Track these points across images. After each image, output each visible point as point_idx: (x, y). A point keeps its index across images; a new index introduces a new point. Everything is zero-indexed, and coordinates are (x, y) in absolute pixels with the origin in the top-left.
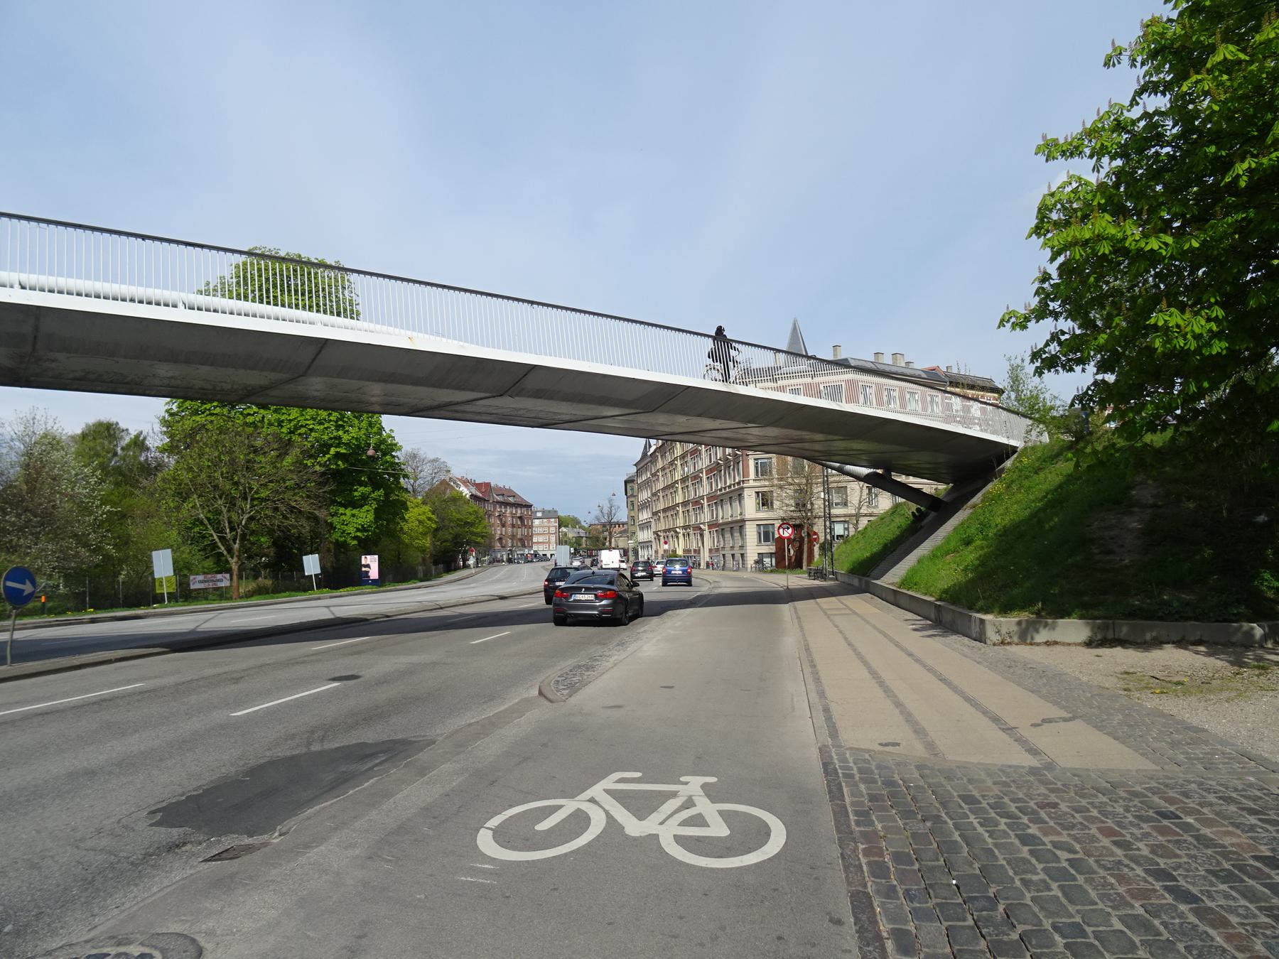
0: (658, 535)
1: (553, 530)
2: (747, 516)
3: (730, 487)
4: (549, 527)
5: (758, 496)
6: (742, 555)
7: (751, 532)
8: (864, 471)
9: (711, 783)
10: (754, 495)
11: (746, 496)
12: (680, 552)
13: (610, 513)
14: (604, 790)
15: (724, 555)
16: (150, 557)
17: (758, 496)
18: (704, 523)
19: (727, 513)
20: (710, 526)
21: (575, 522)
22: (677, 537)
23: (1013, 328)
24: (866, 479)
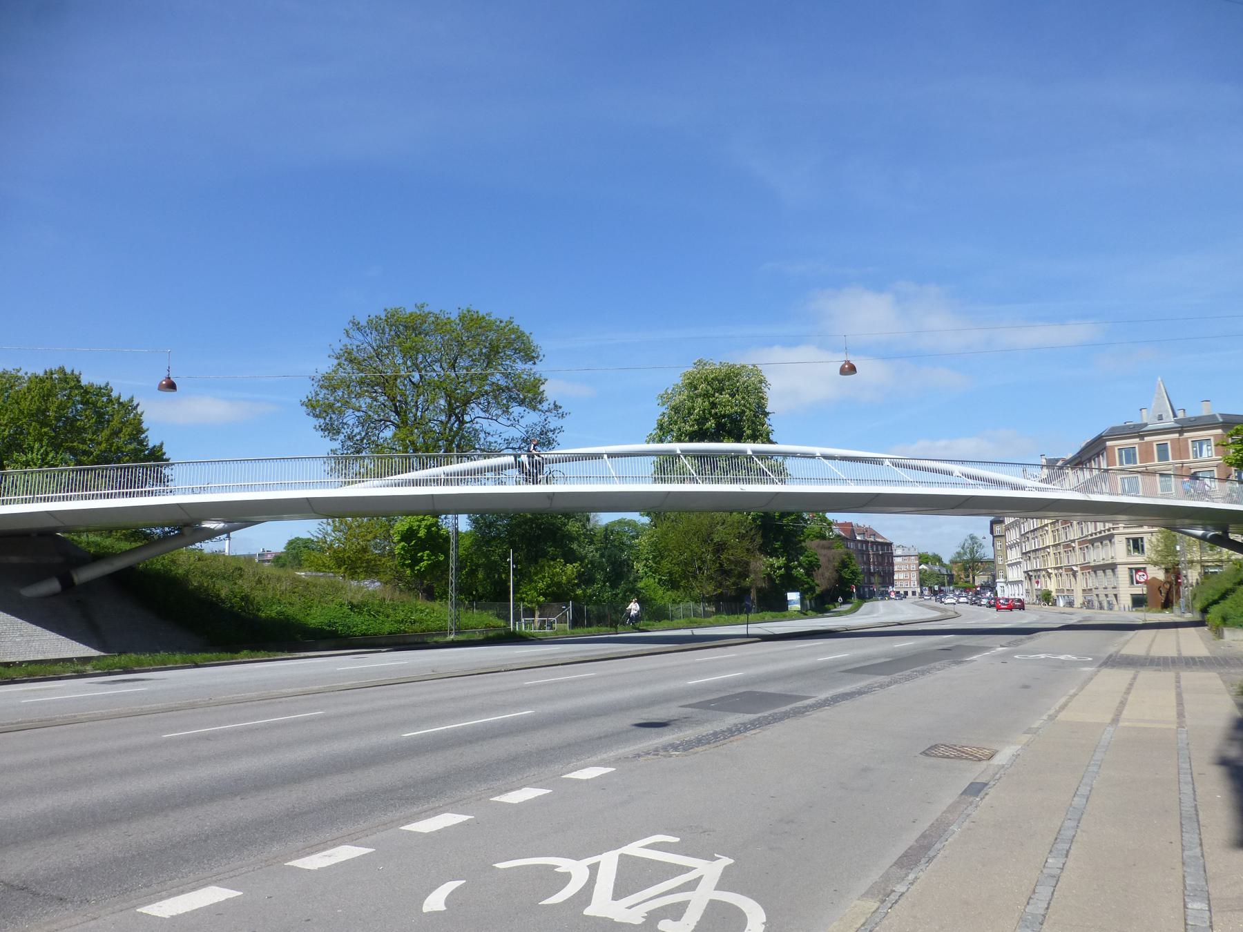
0: (1028, 574)
1: (914, 567)
2: (1118, 560)
3: (1100, 532)
4: (909, 565)
5: (1129, 542)
6: (1116, 596)
7: (1123, 572)
8: (1200, 532)
9: (676, 842)
10: (1125, 541)
11: (1116, 542)
12: (398, 593)
13: (972, 551)
14: (703, 876)
15: (1097, 595)
16: (797, 591)
17: (1129, 542)
18: (1076, 565)
19: (1097, 555)
20: (1082, 569)
21: (937, 559)
22: (1050, 578)
23: (560, 407)
24: (1203, 538)
